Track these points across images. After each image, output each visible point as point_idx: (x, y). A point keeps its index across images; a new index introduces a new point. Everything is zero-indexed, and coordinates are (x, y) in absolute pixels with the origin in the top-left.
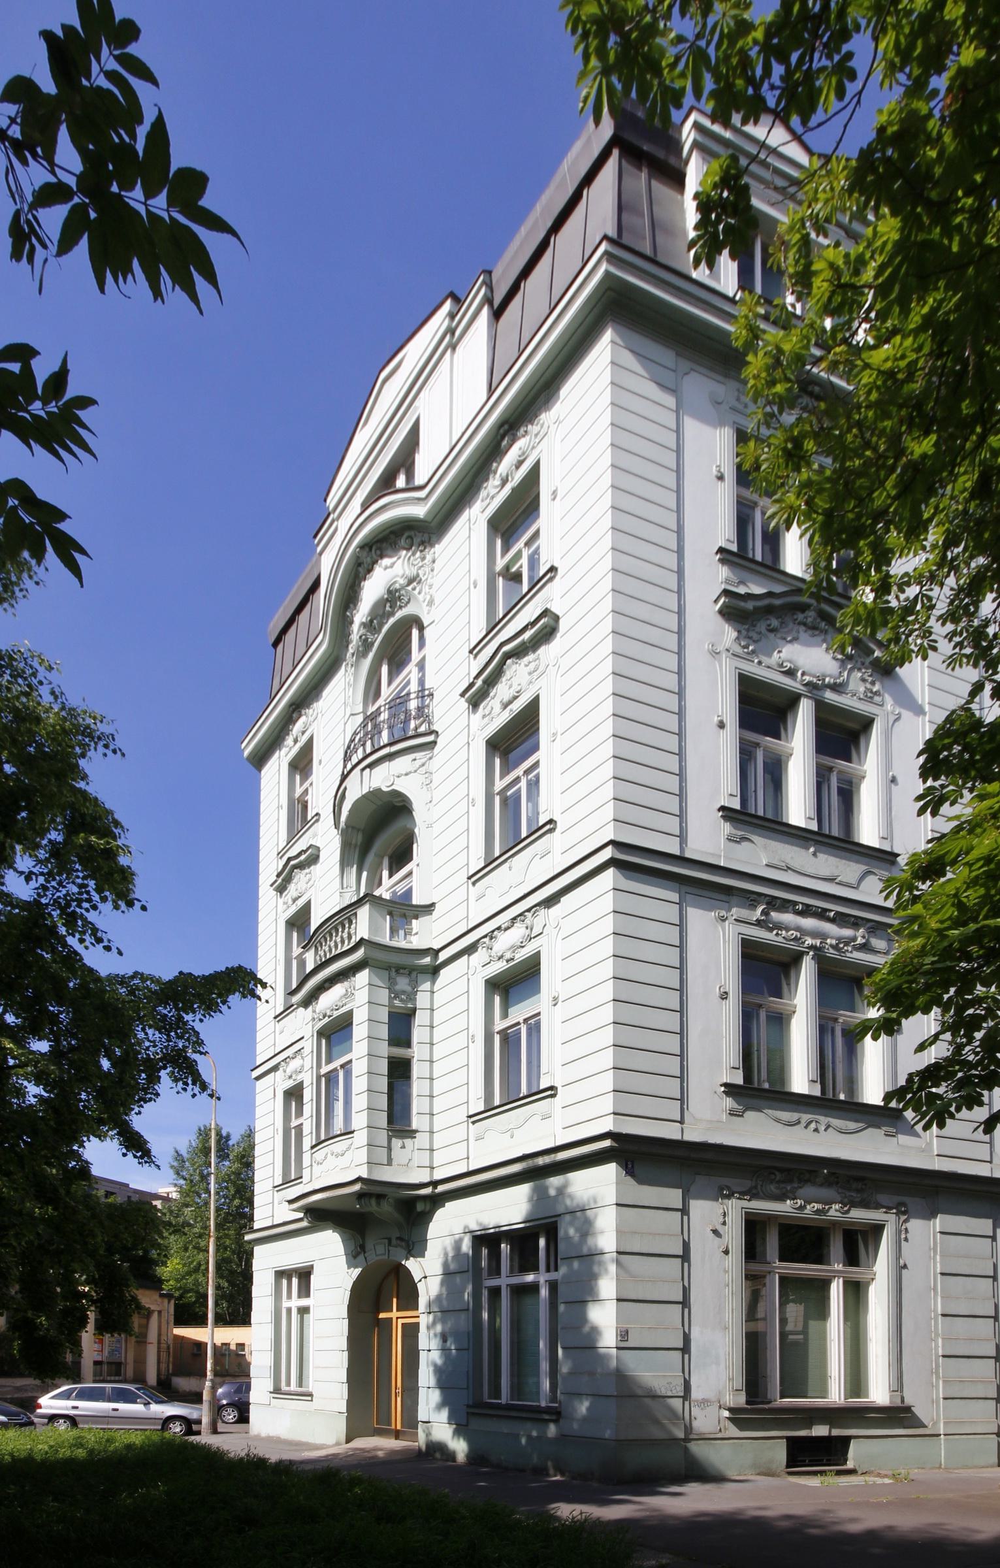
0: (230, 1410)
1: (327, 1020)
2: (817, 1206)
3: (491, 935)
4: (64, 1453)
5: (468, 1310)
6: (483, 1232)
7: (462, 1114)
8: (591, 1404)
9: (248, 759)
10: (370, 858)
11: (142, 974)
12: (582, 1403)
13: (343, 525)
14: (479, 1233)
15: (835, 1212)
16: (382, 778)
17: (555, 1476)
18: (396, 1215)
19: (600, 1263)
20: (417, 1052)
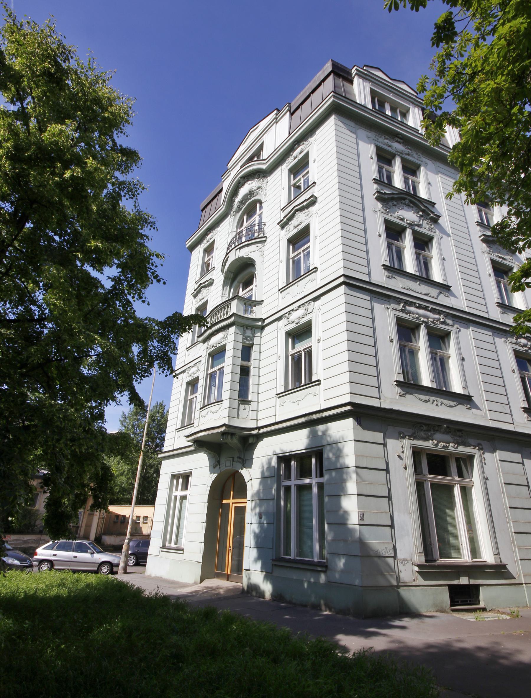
0: (132, 557)
1: (214, 348)
2: (444, 444)
3: (289, 313)
4: (54, 592)
5: (274, 499)
6: (283, 455)
7: (273, 393)
8: (346, 561)
9: (188, 248)
10: (235, 283)
11: (150, 318)
12: (340, 559)
13: (233, 173)
14: (281, 455)
15: (451, 447)
16: (244, 253)
17: (326, 611)
18: (239, 445)
19: (347, 473)
20: (253, 363)
